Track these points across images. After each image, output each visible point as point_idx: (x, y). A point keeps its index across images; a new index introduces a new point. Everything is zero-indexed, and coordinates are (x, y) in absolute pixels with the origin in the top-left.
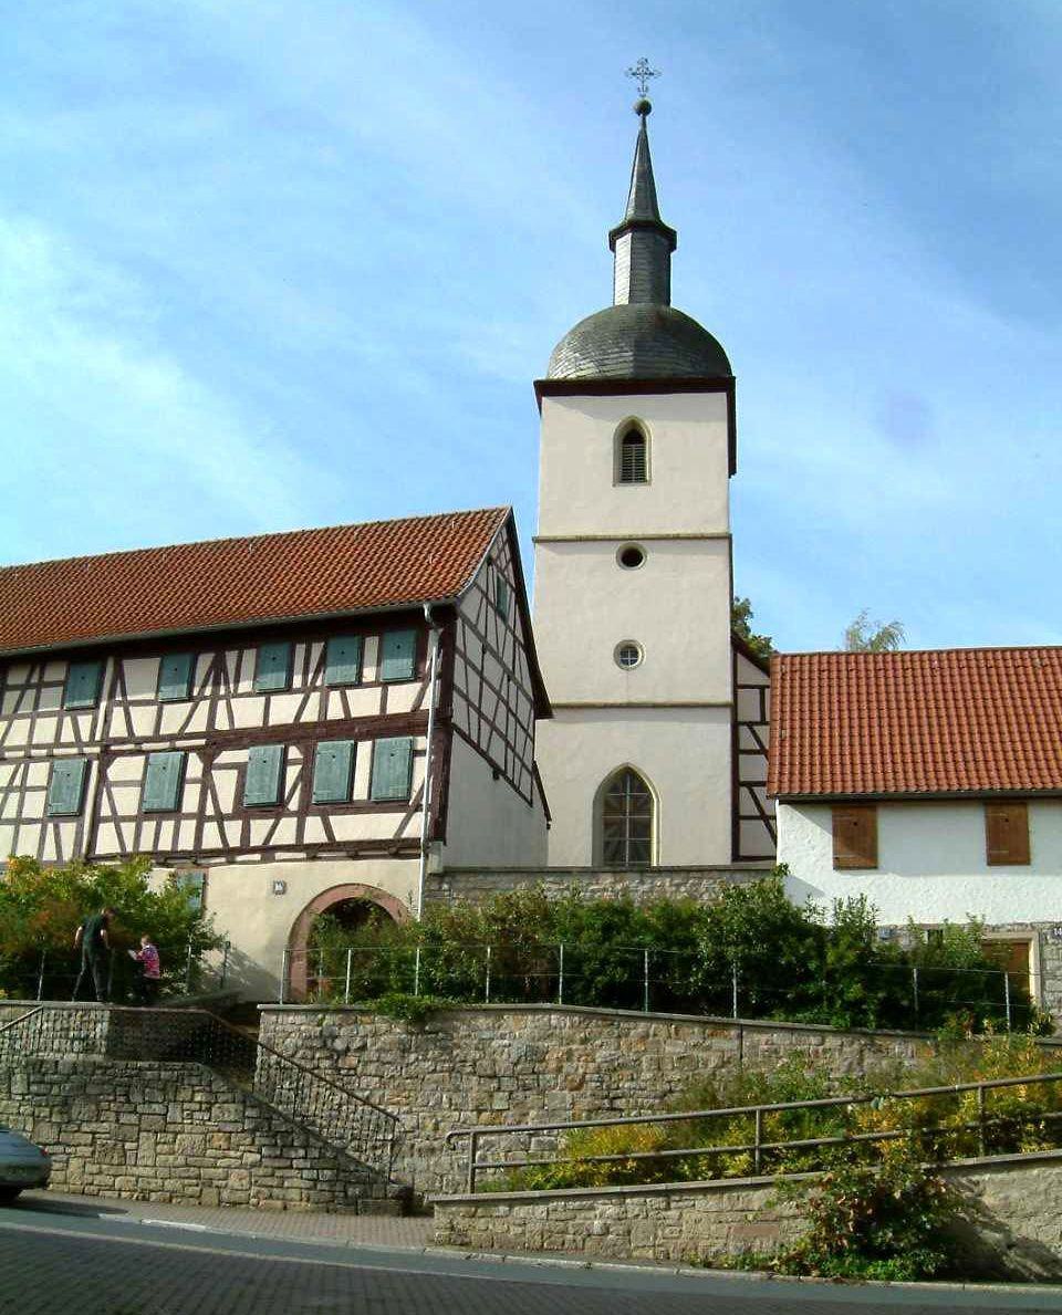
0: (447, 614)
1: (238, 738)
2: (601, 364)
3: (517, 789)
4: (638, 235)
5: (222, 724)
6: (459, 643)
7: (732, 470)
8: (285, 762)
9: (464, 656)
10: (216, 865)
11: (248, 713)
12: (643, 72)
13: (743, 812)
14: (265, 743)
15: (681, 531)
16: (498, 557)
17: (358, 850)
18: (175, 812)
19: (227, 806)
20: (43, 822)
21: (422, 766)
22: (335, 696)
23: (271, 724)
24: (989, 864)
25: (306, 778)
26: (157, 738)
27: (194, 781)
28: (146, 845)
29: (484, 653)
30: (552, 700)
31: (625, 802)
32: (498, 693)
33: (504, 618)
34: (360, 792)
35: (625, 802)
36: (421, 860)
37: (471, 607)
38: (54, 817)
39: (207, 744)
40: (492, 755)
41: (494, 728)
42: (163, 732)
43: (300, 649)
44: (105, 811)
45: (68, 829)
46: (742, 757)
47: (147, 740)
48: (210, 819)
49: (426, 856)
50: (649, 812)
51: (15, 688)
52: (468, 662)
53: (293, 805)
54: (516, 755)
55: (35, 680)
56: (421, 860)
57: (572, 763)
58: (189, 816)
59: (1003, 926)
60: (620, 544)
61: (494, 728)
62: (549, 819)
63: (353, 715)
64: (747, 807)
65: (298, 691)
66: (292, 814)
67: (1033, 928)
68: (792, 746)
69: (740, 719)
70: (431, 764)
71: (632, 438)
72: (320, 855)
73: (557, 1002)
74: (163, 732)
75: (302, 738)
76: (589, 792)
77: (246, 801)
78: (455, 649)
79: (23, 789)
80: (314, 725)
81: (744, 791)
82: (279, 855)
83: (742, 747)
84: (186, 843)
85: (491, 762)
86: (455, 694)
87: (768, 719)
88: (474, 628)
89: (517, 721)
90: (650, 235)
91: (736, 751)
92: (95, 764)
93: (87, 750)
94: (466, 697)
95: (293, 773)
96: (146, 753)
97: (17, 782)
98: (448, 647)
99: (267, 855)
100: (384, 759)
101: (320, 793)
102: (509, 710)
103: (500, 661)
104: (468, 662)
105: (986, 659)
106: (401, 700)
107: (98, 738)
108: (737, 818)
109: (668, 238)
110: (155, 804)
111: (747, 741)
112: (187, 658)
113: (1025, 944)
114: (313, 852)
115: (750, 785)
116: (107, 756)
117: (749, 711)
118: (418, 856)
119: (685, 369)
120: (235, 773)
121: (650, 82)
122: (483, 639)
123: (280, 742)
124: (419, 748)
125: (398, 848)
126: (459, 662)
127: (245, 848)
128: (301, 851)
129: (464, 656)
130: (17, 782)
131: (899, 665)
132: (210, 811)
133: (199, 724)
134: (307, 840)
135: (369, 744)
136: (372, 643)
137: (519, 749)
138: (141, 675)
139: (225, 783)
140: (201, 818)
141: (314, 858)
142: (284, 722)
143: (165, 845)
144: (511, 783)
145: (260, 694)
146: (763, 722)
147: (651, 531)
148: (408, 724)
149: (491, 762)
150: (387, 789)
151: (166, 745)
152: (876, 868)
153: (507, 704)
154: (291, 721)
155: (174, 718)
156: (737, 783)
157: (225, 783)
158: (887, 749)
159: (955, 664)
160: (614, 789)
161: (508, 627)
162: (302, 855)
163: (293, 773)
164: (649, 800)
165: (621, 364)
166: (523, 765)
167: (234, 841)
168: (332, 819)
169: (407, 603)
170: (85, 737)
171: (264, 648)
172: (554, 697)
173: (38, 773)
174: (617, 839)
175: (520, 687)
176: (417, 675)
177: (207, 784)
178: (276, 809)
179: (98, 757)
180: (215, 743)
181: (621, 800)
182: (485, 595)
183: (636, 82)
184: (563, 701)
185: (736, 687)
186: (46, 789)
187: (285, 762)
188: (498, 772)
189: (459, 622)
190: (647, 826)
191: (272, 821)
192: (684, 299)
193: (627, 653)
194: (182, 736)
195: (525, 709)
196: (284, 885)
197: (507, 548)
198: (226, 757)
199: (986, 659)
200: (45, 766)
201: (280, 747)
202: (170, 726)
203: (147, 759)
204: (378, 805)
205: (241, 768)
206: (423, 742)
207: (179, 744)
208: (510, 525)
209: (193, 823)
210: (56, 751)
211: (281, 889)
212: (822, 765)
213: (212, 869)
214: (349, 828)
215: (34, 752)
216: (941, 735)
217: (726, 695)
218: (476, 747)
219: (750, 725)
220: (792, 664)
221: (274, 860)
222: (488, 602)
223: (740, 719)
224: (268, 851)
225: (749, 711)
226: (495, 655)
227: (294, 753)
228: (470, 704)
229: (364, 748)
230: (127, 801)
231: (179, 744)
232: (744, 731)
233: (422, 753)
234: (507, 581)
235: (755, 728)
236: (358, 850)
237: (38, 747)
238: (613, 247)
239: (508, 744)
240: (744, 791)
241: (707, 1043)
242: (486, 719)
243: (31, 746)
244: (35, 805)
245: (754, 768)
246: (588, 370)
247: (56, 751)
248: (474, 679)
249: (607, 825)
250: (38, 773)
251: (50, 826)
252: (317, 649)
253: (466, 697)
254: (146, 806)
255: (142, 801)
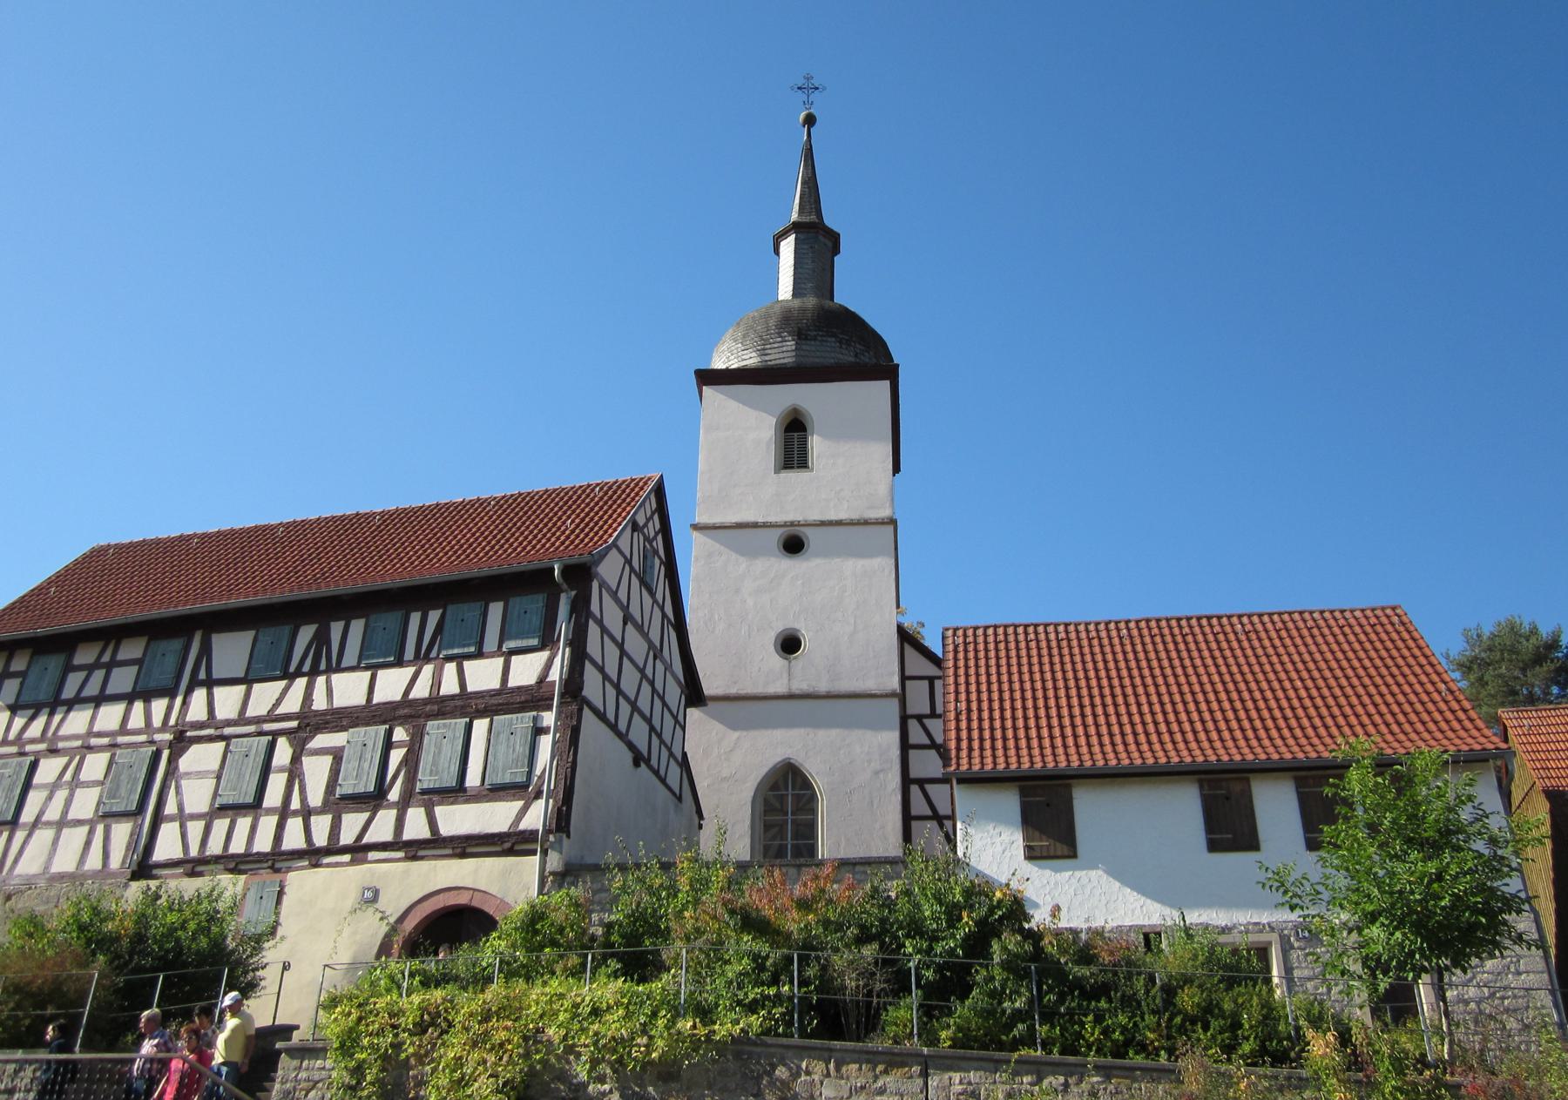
0: (581, 574)
1: (339, 719)
2: (762, 352)
3: (663, 781)
4: (802, 236)
5: (320, 703)
6: (595, 607)
7: (896, 468)
8: (388, 745)
9: (600, 623)
10: (298, 869)
11: (348, 689)
12: (808, 88)
13: (913, 740)
14: (368, 724)
15: (843, 516)
16: (646, 525)
17: (465, 846)
18: (255, 806)
19: (316, 798)
20: (92, 824)
21: (546, 743)
22: (450, 669)
23: (375, 701)
24: (1214, 846)
25: (411, 762)
26: (242, 720)
27: (281, 770)
28: (215, 847)
29: (625, 623)
30: (706, 692)
31: (786, 801)
32: (642, 671)
33: (652, 594)
34: (473, 779)
35: (786, 801)
36: (537, 858)
37: (610, 569)
38: (108, 816)
39: (299, 726)
40: (631, 736)
41: (634, 707)
42: (250, 713)
43: (415, 618)
44: (171, 808)
45: (122, 832)
46: (912, 753)
47: (229, 723)
48: (295, 813)
49: (545, 853)
50: (814, 811)
51: (80, 668)
52: (604, 630)
53: (394, 795)
54: (662, 742)
55: (106, 658)
56: (537, 858)
57: (727, 764)
58: (270, 811)
59: (1234, 926)
60: (780, 531)
61: (634, 707)
62: (701, 817)
63: (469, 689)
64: (919, 806)
65: (409, 664)
66: (390, 806)
67: (1272, 929)
68: (969, 720)
69: (910, 711)
70: (554, 743)
71: (794, 430)
72: (421, 853)
73: (71, 1051)
74: (250, 713)
75: (411, 716)
76: (746, 792)
77: (339, 792)
78: (589, 614)
79: (76, 784)
80: (425, 702)
81: (915, 790)
82: (372, 855)
83: (914, 813)
84: (263, 844)
85: (631, 746)
86: (588, 664)
87: (939, 710)
88: (614, 595)
89: (665, 704)
90: (818, 242)
91: (905, 746)
92: (166, 753)
93: (158, 737)
94: (601, 669)
95: (396, 756)
96: (226, 738)
97: (68, 776)
98: (581, 609)
99: (360, 855)
100: (503, 737)
101: (425, 780)
102: (654, 690)
103: (645, 636)
104: (604, 630)
105: (1180, 627)
106: (526, 670)
107: (172, 722)
108: (907, 818)
109: (833, 241)
110: (228, 797)
111: (916, 735)
112: (286, 630)
113: (1263, 952)
114: (414, 850)
115: (922, 783)
116: (181, 742)
117: (919, 704)
118: (533, 853)
119: (847, 357)
120: (329, 759)
121: (815, 96)
122: (625, 609)
123: (384, 723)
124: (545, 724)
125: (511, 843)
126: (593, 630)
127: (333, 849)
128: (398, 850)
129: (600, 623)
130: (68, 776)
131: (1083, 635)
132: (295, 804)
133: (292, 704)
134: (407, 836)
135: (486, 721)
136: (496, 610)
137: (667, 737)
138: (231, 650)
139: (316, 771)
140: (284, 813)
141: (415, 858)
142: (389, 699)
143: (238, 847)
144: (656, 773)
145: (367, 668)
146: (933, 714)
147: (815, 516)
148: (533, 698)
149: (631, 746)
150: (504, 772)
151: (252, 729)
152: (1074, 855)
153: (652, 683)
154: (398, 698)
155: (264, 695)
156: (907, 781)
157: (316, 771)
158: (1078, 721)
159: (1145, 632)
160: (775, 787)
161: (655, 601)
162: (401, 854)
163: (396, 756)
164: (813, 798)
165: (784, 352)
166: (671, 754)
167: (320, 840)
168: (438, 810)
169: (543, 571)
170: (157, 721)
171: (373, 617)
172: (709, 687)
173: (95, 765)
174: (777, 842)
175: (668, 668)
176: (547, 641)
177: (295, 772)
178: (373, 800)
179: (171, 745)
180: (310, 723)
181: (782, 798)
182: (629, 561)
183: (801, 96)
184: (720, 692)
185: (904, 679)
186: (102, 783)
187: (388, 745)
188: (638, 759)
189: (595, 585)
190: (812, 826)
191: (366, 815)
192: (845, 295)
193: (790, 644)
194: (271, 717)
195: (674, 694)
196: (376, 892)
197: (656, 517)
198: (322, 740)
199: (1180, 627)
200: (104, 757)
201: (383, 728)
202: (257, 708)
203: (228, 746)
204: (496, 791)
205: (337, 755)
206: (549, 718)
207: (267, 727)
208: (659, 491)
209: (274, 819)
210: (121, 739)
211: (372, 897)
212: (1005, 739)
213: (291, 875)
214: (457, 819)
215: (94, 741)
216: (1139, 705)
217: (894, 683)
218: (614, 727)
219: (920, 718)
220: (965, 636)
221: (365, 861)
222: (632, 569)
223: (910, 711)
224: (359, 851)
225: (918, 701)
226: (639, 628)
227: (400, 734)
228: (606, 677)
229: (480, 726)
230: (196, 795)
231: (267, 727)
232: (913, 725)
233: (545, 731)
234: (656, 552)
235: (926, 721)
236: (465, 846)
237: (100, 735)
238: (777, 251)
239: (652, 729)
240: (915, 789)
241: (880, 1083)
242: (627, 698)
243: (90, 733)
244: (85, 804)
245: (926, 764)
246: (751, 359)
247: (121, 739)
248: (612, 653)
249: (767, 827)
250: (95, 765)
251: (100, 828)
252: (434, 616)
253: (601, 669)
254: (219, 801)
255: (216, 794)
